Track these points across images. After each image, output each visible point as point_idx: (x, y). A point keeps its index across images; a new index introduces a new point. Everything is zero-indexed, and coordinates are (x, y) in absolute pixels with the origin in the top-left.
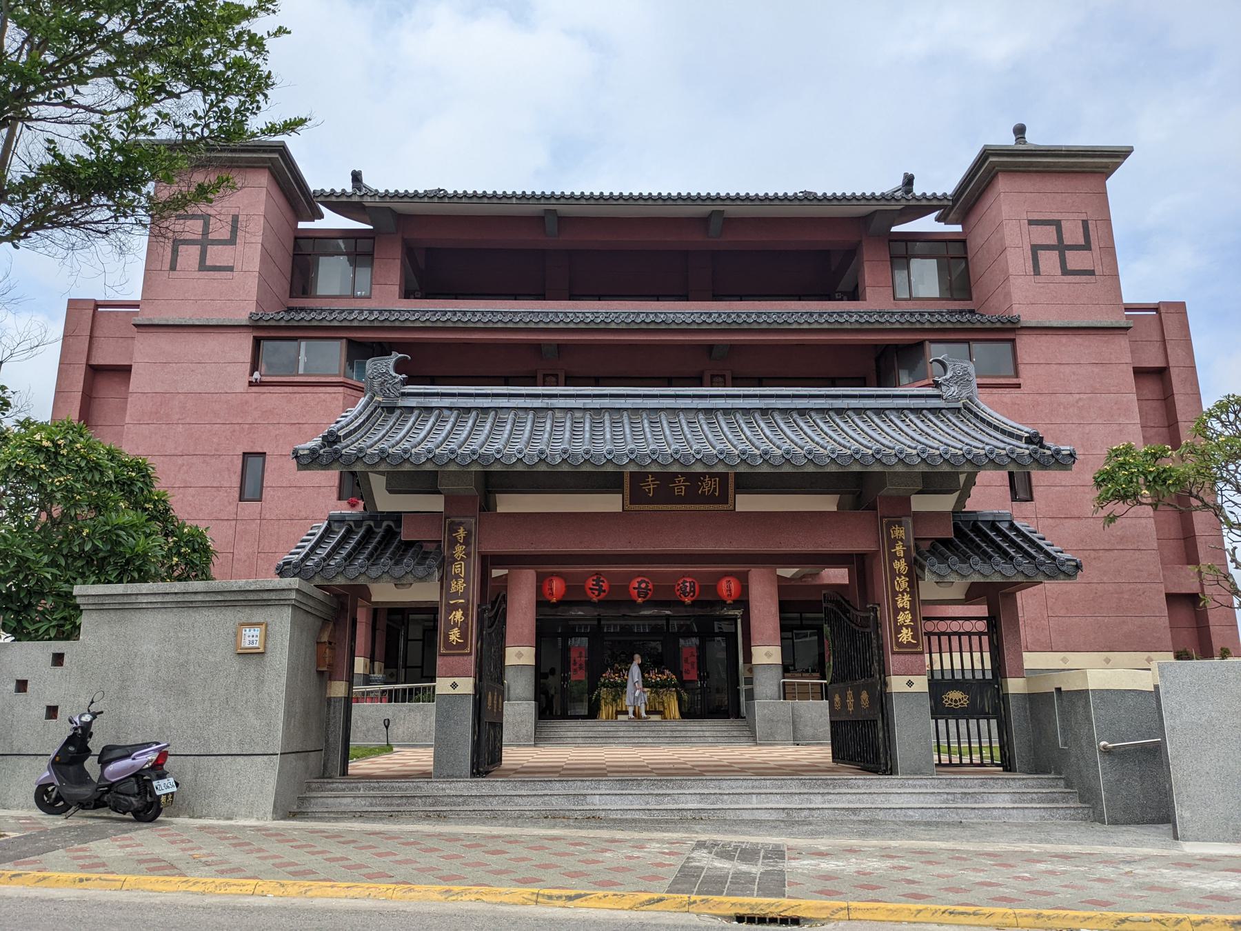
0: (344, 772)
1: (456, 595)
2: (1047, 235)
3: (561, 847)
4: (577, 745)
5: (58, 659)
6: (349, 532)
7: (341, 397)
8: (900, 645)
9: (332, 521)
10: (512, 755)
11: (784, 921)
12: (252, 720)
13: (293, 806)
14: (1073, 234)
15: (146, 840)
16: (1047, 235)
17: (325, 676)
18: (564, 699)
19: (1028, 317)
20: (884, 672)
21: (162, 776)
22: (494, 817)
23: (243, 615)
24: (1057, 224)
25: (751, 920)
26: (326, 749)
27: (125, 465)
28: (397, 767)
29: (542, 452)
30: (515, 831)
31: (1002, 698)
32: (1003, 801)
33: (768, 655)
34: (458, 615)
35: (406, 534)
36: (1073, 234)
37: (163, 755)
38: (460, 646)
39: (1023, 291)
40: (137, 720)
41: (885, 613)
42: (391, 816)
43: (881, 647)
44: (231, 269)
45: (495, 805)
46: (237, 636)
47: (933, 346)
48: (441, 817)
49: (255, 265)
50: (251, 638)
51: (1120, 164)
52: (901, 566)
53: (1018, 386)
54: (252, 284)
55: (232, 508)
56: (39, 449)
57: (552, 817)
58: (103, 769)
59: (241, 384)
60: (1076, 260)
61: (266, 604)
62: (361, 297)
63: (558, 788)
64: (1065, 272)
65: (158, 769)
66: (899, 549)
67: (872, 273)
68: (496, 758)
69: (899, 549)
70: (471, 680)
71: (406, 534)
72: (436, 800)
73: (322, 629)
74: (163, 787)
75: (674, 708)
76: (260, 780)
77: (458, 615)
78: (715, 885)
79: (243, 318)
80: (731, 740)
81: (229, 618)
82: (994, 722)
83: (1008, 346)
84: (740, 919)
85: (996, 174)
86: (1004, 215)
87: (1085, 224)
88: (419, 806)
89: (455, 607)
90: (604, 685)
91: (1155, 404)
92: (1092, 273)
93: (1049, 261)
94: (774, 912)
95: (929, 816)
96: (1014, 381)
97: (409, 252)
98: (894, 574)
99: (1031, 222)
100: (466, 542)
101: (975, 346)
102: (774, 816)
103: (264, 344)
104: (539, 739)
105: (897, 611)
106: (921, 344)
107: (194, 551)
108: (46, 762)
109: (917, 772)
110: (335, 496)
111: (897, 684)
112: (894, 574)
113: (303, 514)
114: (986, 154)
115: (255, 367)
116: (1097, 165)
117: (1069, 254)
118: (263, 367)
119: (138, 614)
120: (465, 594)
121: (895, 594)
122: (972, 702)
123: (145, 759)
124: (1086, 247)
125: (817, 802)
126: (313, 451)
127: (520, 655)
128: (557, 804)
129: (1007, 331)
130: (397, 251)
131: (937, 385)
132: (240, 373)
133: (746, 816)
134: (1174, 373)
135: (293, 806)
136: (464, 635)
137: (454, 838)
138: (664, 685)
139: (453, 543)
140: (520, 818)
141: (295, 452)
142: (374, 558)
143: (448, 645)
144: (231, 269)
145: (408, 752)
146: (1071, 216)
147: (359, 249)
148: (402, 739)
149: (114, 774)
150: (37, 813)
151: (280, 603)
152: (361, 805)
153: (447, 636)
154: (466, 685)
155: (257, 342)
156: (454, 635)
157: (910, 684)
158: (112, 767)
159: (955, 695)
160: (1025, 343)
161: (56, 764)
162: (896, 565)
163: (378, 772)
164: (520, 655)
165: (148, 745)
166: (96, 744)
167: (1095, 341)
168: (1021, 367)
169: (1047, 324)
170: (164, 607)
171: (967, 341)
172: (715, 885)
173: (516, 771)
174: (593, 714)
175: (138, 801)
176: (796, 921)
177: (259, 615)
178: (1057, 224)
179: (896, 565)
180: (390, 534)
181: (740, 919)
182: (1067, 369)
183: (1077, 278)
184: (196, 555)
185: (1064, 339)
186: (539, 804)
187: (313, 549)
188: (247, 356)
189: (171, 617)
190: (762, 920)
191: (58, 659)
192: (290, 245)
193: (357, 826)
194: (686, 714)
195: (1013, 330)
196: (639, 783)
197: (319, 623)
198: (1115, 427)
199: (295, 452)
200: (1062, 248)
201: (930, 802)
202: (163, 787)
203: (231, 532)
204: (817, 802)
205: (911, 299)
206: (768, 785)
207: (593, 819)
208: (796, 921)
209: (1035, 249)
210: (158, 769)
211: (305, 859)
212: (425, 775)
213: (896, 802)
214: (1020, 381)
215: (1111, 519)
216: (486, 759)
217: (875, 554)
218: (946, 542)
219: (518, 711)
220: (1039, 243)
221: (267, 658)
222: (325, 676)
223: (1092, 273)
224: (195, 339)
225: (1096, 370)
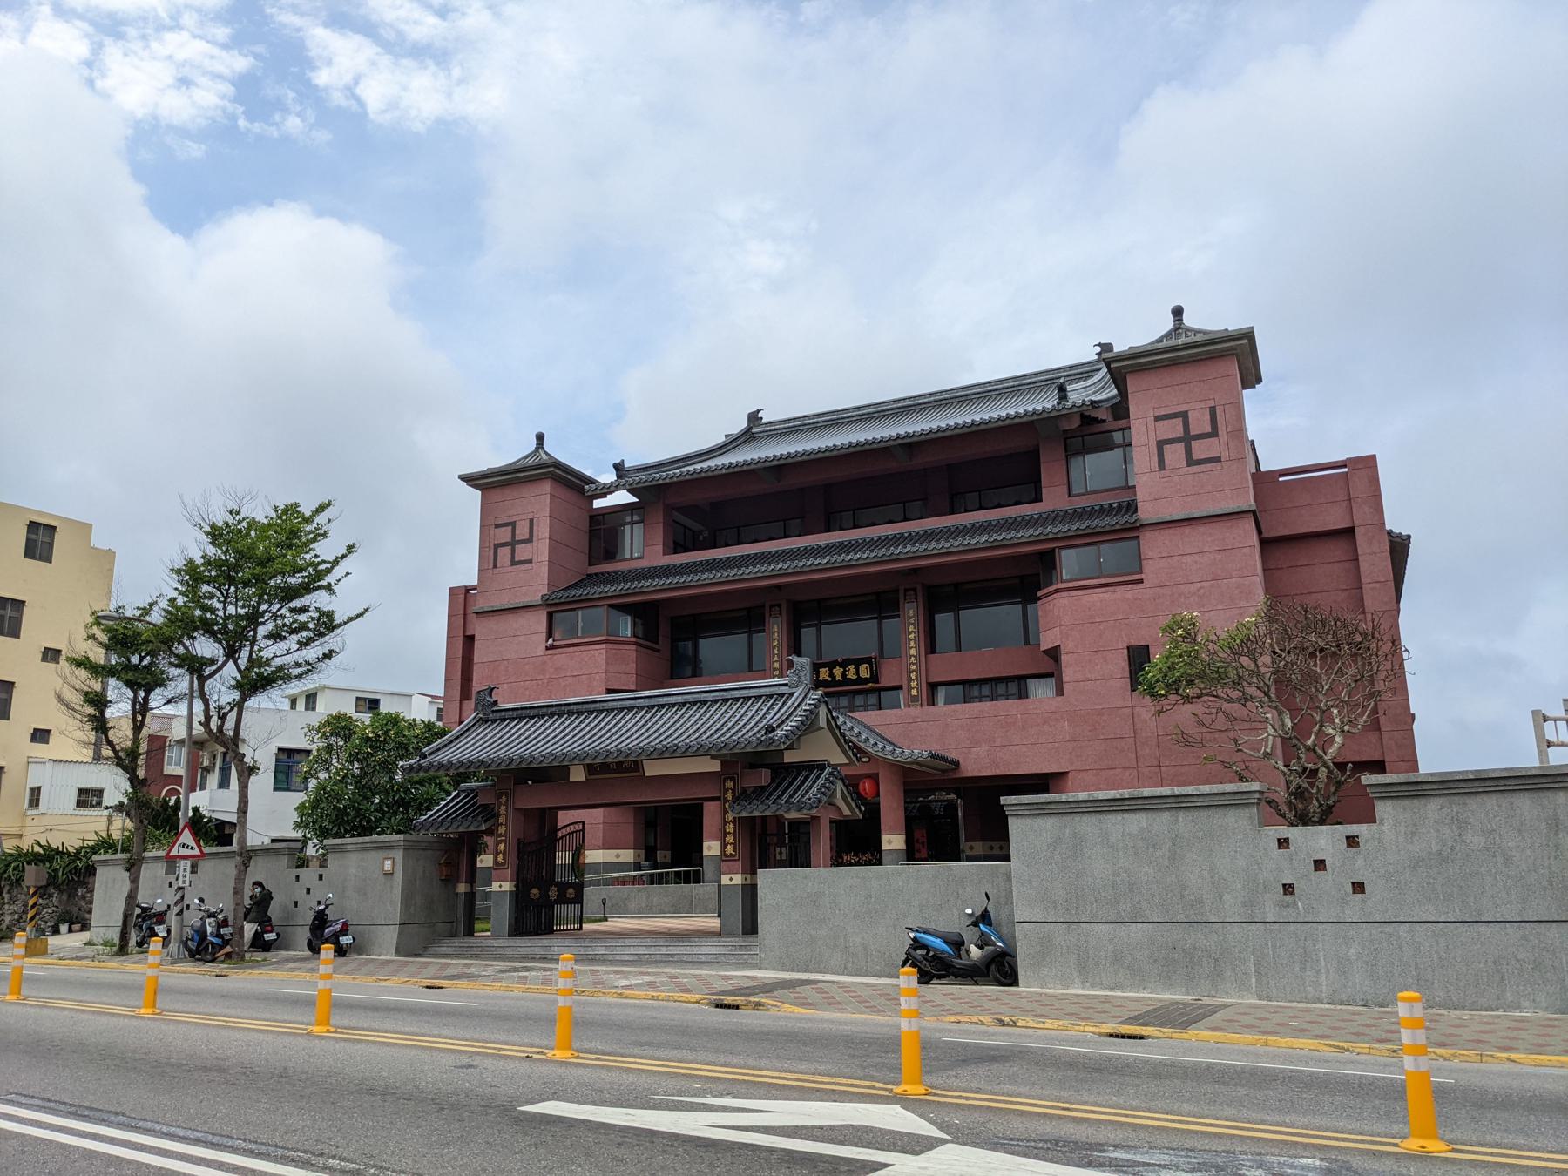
11: (1135, 1037)
14: (1200, 423)
16: (1174, 429)
17: (449, 880)
24: (1184, 415)
25: (1117, 1036)
36: (1200, 423)
39: (1157, 487)
44: (530, 561)
47: (1064, 552)
49: (545, 557)
50: (388, 865)
53: (1141, 581)
54: (545, 570)
59: (541, 650)
61: (392, 848)
64: (1191, 462)
67: (1050, 474)
76: (390, 936)
79: (538, 599)
81: (381, 854)
84: (1111, 1035)
87: (1213, 410)
88: (475, 951)
92: (1218, 459)
93: (1175, 454)
97: (669, 509)
99: (1157, 418)
101: (1103, 547)
103: (556, 616)
115: (550, 634)
117: (1194, 444)
118: (557, 636)
132: (539, 641)
139: (500, 804)
144: (530, 561)
146: (1198, 405)
151: (398, 848)
155: (550, 616)
176: (1141, 1038)
177: (392, 854)
178: (1184, 415)
181: (1111, 1035)
182: (1189, 559)
183: (1203, 467)
185: (1187, 530)
188: (543, 627)
190: (1123, 1037)
192: (585, 525)
195: (1137, 528)
208: (1141, 1038)
209: (1161, 445)
222: (449, 880)
223: (1218, 459)
224: (510, 617)
225: (1219, 557)
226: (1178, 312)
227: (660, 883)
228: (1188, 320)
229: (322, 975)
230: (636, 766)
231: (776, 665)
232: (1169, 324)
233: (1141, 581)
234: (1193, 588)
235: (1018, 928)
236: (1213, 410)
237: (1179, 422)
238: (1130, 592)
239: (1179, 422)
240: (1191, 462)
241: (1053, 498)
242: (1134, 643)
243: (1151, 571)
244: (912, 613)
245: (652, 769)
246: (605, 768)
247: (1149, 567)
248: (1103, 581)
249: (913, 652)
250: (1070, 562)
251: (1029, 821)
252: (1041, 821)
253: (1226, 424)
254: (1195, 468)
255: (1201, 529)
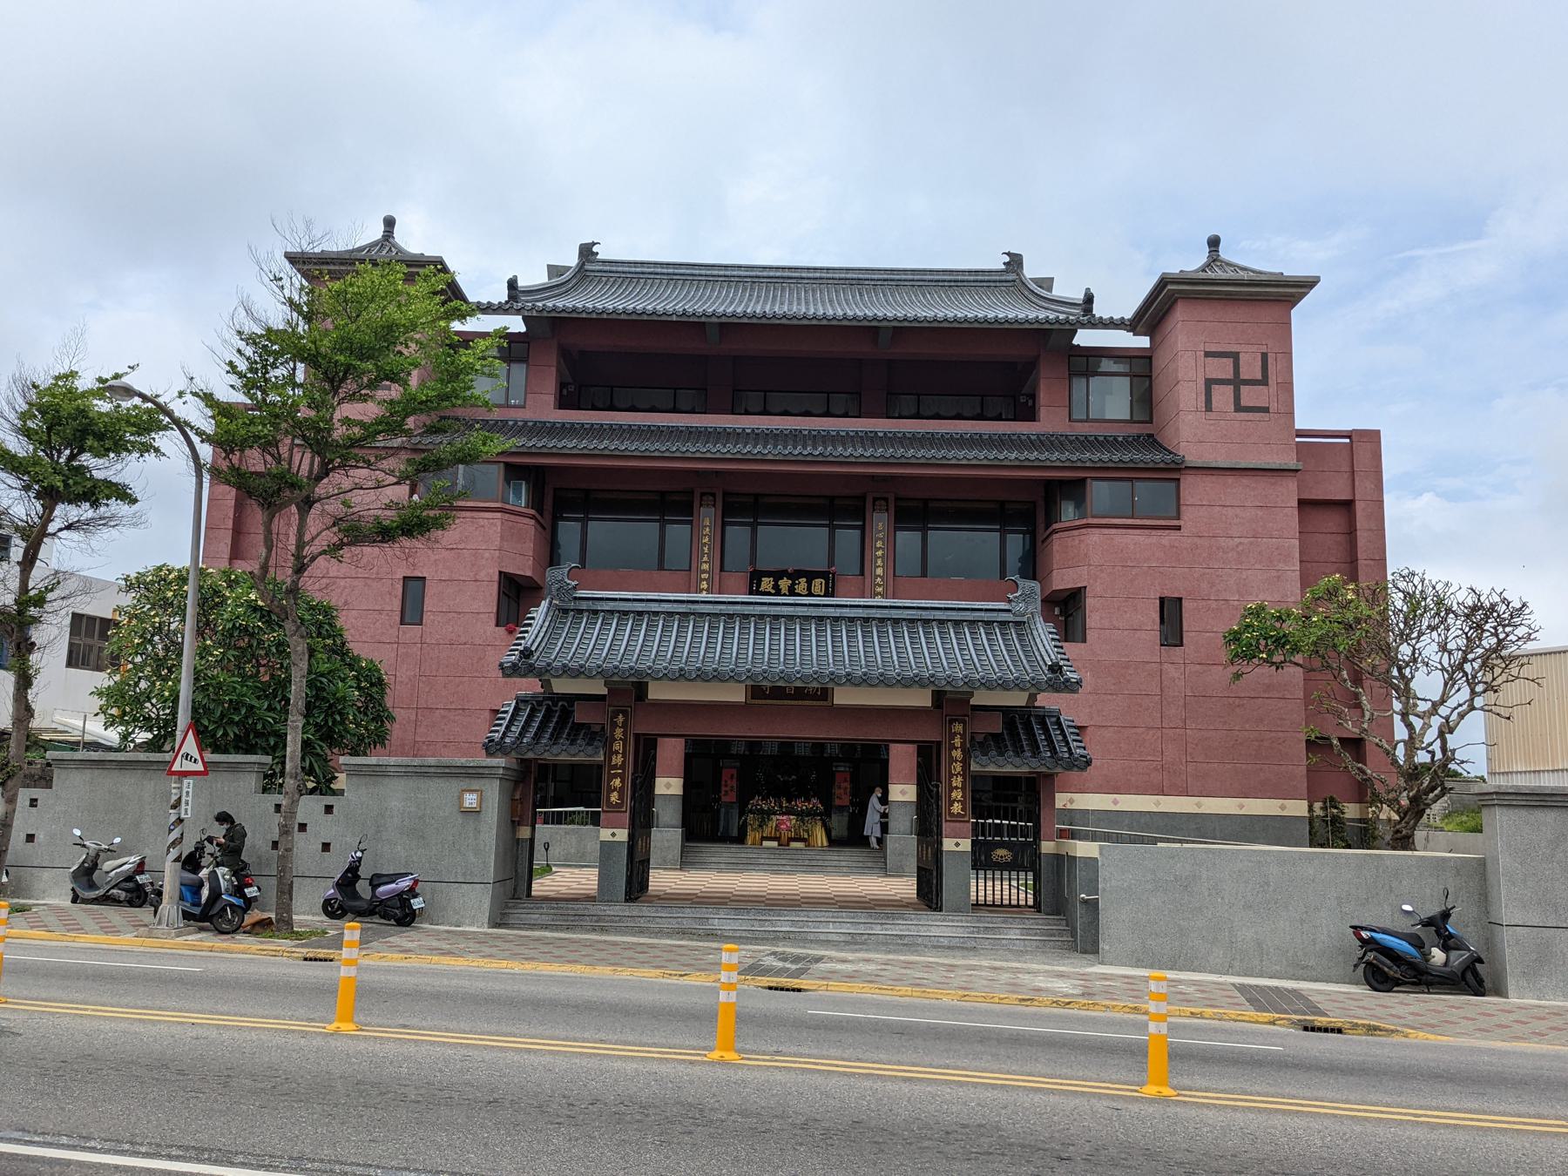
0: (529, 895)
1: (615, 767)
2: (1223, 369)
3: (682, 951)
4: (720, 871)
5: (329, 809)
6: (533, 710)
7: (499, 523)
8: (952, 815)
9: (521, 701)
10: (662, 880)
12: (472, 859)
13: (499, 920)
14: (1250, 369)
15: (402, 938)
16: (1223, 369)
18: (706, 827)
19: (1191, 453)
20: (940, 834)
21: (415, 896)
22: (641, 932)
23: (464, 784)
24: (1235, 356)
26: (516, 876)
27: (313, 608)
28: (564, 890)
29: (681, 669)
30: (656, 941)
31: (1037, 854)
32: (1014, 935)
33: (903, 793)
34: (617, 782)
35: (580, 716)
36: (1250, 369)
37: (416, 882)
38: (620, 805)
39: (1193, 430)
40: (395, 855)
41: (943, 789)
42: (568, 929)
43: (939, 815)
45: (642, 923)
46: (460, 799)
48: (603, 930)
50: (470, 800)
51: (1305, 294)
52: (957, 754)
53: (1178, 528)
55: (394, 632)
56: (256, 609)
57: (683, 933)
58: (373, 890)
60: (1249, 396)
61: (480, 776)
62: (515, 406)
63: (688, 912)
64: (1239, 408)
65: (412, 892)
66: (957, 741)
68: (644, 885)
69: (957, 741)
70: (626, 832)
71: (580, 716)
72: (599, 918)
73: (515, 790)
74: (417, 903)
75: (820, 837)
76: (480, 900)
77: (617, 782)
78: (767, 971)
80: (862, 870)
81: (455, 785)
82: (1030, 876)
83: (1173, 485)
85: (1176, 300)
86: (1179, 346)
87: (1264, 356)
89: (615, 776)
90: (751, 812)
91: (1340, 538)
92: (1266, 410)
93: (1222, 396)
94: (789, 985)
95: (954, 942)
96: (1175, 523)
97: (565, 354)
98: (952, 760)
99: (1207, 354)
100: (624, 725)
101: (1138, 484)
102: (843, 938)
104: (685, 862)
105: (952, 789)
106: (1084, 480)
107: (372, 685)
108: (330, 883)
109: (957, 910)
110: (494, 622)
111: (948, 844)
112: (952, 760)
113: (463, 639)
114: (1164, 282)
116: (1282, 294)
117: (1244, 389)
119: (386, 781)
120: (623, 767)
121: (951, 775)
122: (1015, 857)
123: (404, 884)
124: (1262, 380)
125: (877, 930)
126: (514, 665)
127: (668, 786)
128: (686, 924)
129: (1174, 471)
130: (553, 358)
131: (1010, 601)
133: (822, 937)
134: (1359, 507)
135: (499, 920)
136: (621, 797)
137: (615, 944)
138: (811, 813)
139: (614, 725)
140: (659, 933)
141: (501, 665)
142: (555, 738)
143: (609, 804)
145: (566, 872)
147: (513, 349)
148: (571, 870)
149: (383, 893)
150: (324, 918)
152: (545, 919)
153: (608, 798)
154: (622, 835)
156: (614, 797)
157: (957, 845)
158: (381, 889)
159: (1001, 852)
160: (1189, 483)
161: (338, 885)
162: (954, 753)
163: (552, 894)
164: (668, 786)
165: (406, 874)
166: (365, 872)
167: (1261, 485)
168: (1183, 508)
169: (1214, 465)
170: (406, 775)
171: (1131, 479)
172: (767, 971)
173: (659, 898)
174: (740, 839)
175: (399, 913)
176: (799, 990)
177: (476, 784)
178: (1235, 356)
179: (954, 753)
180: (566, 714)
183: (1250, 416)
184: (374, 689)
185: (1230, 480)
186: (674, 924)
187: (508, 728)
189: (412, 783)
191: (329, 809)
193: (548, 934)
194: (834, 842)
196: (749, 911)
197: (512, 785)
198: (1274, 574)
199: (501, 665)
200: (1237, 382)
201: (960, 933)
202: (417, 903)
203: (393, 655)
204: (877, 930)
205: (1087, 420)
206: (845, 916)
207: (711, 935)
208: (799, 990)
209: (1210, 383)
210: (412, 892)
211: (532, 953)
212: (589, 898)
213: (935, 932)
214: (1181, 523)
215: (1238, 676)
216: (636, 887)
217: (939, 743)
218: (996, 737)
219: (666, 836)
220: (1214, 376)
221: (482, 815)
222: (515, 824)
223: (1266, 410)
226: (1214, 243)
227: (559, 823)
228: (1225, 253)
229: (359, 953)
230: (824, 694)
231: (705, 567)
232: (377, 233)
233: (1178, 528)
234: (1231, 543)
235: (1507, 935)
236: (1264, 356)
237: (1229, 362)
238: (1168, 538)
239: (1229, 362)
240: (1239, 408)
241: (1050, 421)
242: (1167, 594)
243: (1189, 517)
244: (707, 518)
245: (842, 697)
246: (778, 693)
247: (1187, 513)
248: (1129, 522)
249: (879, 571)
250: (1099, 492)
251: (1523, 812)
252: (1539, 815)
253: (1274, 370)
254: (1243, 415)
255: (1245, 481)
